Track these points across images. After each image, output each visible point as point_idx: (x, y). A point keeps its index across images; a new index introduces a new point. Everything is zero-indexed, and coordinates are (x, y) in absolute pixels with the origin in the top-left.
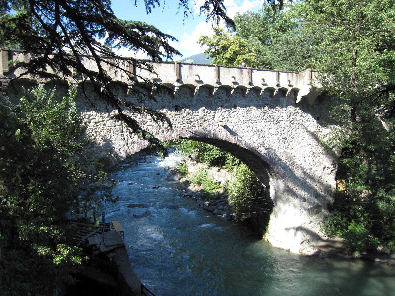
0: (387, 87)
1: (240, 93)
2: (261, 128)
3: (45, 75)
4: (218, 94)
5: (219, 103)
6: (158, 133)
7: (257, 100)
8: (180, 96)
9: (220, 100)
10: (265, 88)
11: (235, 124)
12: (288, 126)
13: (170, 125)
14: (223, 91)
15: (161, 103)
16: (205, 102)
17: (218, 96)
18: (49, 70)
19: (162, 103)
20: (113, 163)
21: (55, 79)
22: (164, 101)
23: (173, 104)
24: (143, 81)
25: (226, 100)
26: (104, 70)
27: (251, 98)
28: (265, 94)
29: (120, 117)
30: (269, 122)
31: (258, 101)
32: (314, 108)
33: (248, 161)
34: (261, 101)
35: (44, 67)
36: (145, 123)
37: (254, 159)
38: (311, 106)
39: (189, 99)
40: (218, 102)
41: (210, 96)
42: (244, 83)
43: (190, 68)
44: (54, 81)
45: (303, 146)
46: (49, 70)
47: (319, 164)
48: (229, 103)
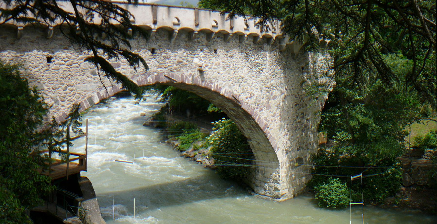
0: (347, 60)
1: (222, 38)
2: (242, 75)
3: (24, 20)
4: (198, 38)
5: (199, 47)
6: (133, 77)
7: (239, 46)
8: (158, 39)
9: (200, 44)
10: (248, 34)
11: (215, 70)
12: (272, 74)
13: (146, 67)
14: (203, 35)
15: (137, 46)
16: (184, 46)
17: (198, 40)
18: (30, 15)
19: (138, 46)
20: (86, 107)
21: (34, 22)
22: (140, 44)
23: (149, 47)
24: (168, 80)
25: (206, 44)
26: (79, 13)
27: (233, 44)
28: (249, 40)
29: (96, 60)
30: (252, 70)
31: (241, 47)
32: (299, 57)
33: (228, 110)
34: (243, 47)
35: (25, 13)
36: (119, 66)
37: (234, 108)
38: (296, 55)
39: (166, 42)
40: (197, 47)
41: (189, 39)
42: (227, 28)
43: (169, 12)
44: (33, 24)
45: (287, 96)
46: (30, 15)
47: (302, 115)
48: (209, 48)
